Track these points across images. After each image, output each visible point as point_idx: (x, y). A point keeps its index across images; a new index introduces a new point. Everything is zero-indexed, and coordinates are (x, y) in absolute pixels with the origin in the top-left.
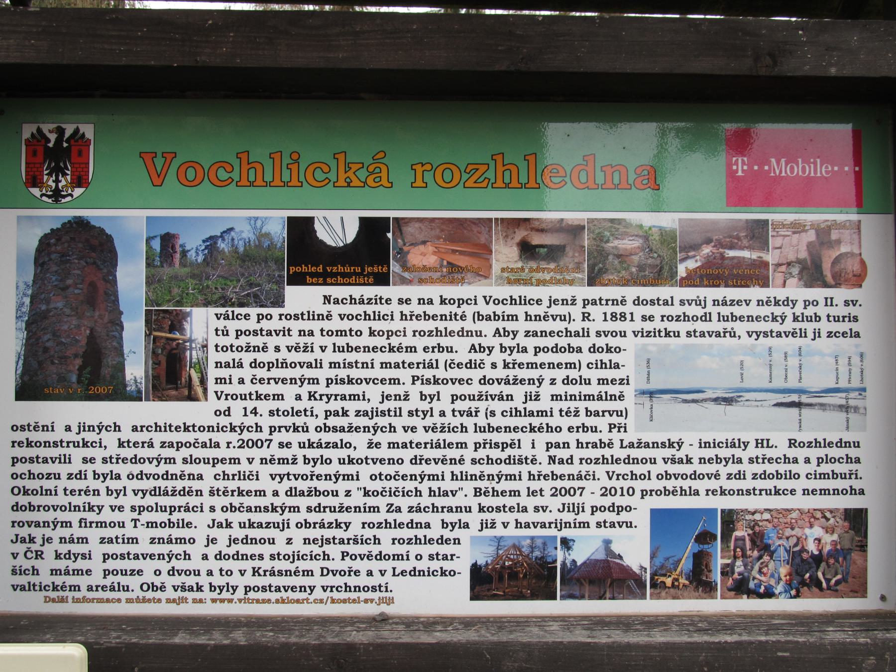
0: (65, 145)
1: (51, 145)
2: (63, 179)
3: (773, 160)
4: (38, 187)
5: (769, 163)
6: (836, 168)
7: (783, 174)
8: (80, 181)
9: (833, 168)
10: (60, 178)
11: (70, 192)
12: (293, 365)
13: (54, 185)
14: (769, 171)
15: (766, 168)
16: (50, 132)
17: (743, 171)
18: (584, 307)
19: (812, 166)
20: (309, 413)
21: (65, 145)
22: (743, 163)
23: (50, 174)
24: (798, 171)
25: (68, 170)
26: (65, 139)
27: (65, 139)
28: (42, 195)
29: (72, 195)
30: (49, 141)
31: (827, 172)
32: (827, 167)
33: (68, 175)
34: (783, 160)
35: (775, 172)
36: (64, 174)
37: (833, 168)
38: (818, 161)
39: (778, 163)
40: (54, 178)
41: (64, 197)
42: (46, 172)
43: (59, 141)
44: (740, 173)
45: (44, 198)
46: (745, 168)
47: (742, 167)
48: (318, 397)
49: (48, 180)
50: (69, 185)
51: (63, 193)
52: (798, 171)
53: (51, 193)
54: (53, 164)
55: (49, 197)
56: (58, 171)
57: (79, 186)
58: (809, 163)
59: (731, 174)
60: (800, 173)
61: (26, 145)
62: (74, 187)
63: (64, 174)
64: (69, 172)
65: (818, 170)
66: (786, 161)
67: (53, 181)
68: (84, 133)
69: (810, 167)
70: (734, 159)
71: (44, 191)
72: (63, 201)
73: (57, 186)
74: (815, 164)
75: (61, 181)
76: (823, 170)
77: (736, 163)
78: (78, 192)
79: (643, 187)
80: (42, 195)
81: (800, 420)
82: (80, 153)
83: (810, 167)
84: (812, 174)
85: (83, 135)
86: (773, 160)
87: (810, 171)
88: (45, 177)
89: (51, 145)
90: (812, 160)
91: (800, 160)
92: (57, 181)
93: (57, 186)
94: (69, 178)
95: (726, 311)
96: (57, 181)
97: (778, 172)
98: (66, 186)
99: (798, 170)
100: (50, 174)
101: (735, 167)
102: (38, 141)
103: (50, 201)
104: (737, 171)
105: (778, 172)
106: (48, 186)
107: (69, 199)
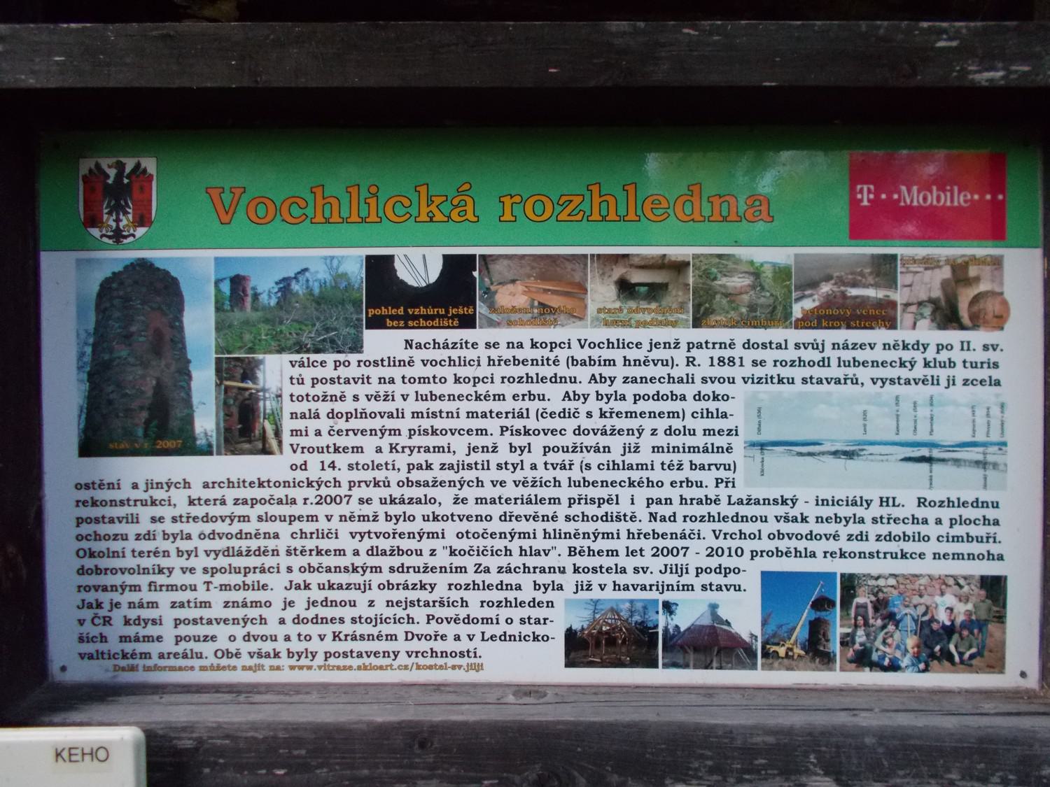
0: (126, 181)
1: (110, 181)
3: (904, 188)
5: (899, 193)
7: (915, 203)
8: (143, 219)
9: (972, 197)
10: (121, 217)
11: (132, 231)
13: (114, 225)
14: (899, 200)
15: (896, 196)
17: (869, 200)
18: (689, 351)
19: (948, 194)
20: (390, 467)
21: (126, 181)
22: (869, 191)
23: (110, 213)
24: (918, 197)
26: (125, 174)
28: (102, 236)
29: (133, 236)
30: (108, 177)
31: (965, 201)
32: (965, 196)
33: (129, 213)
34: (915, 189)
35: (905, 202)
36: (126, 213)
37: (972, 197)
38: (956, 189)
39: (909, 191)
40: (114, 217)
41: (126, 237)
42: (105, 211)
43: (120, 175)
45: (105, 240)
46: (872, 196)
48: (343, 638)
49: (108, 219)
50: (131, 224)
51: (124, 233)
52: (946, 200)
54: (113, 203)
55: (109, 237)
56: (118, 209)
57: (142, 225)
58: (944, 191)
59: (854, 203)
60: (935, 203)
62: (136, 227)
63: (126, 213)
64: (130, 211)
69: (946, 196)
70: (859, 187)
71: (104, 232)
72: (125, 241)
73: (118, 226)
74: (952, 192)
75: (121, 221)
76: (962, 199)
77: (861, 191)
78: (141, 231)
80: (102, 236)
83: (946, 196)
84: (948, 204)
85: (145, 170)
86: (904, 188)
87: (945, 200)
88: (105, 217)
89: (110, 181)
90: (948, 188)
91: (934, 188)
93: (118, 226)
94: (130, 217)
96: (118, 221)
98: (127, 225)
99: (932, 199)
100: (110, 213)
101: (859, 196)
103: (110, 242)
104: (861, 200)
105: (908, 201)
107: (131, 239)
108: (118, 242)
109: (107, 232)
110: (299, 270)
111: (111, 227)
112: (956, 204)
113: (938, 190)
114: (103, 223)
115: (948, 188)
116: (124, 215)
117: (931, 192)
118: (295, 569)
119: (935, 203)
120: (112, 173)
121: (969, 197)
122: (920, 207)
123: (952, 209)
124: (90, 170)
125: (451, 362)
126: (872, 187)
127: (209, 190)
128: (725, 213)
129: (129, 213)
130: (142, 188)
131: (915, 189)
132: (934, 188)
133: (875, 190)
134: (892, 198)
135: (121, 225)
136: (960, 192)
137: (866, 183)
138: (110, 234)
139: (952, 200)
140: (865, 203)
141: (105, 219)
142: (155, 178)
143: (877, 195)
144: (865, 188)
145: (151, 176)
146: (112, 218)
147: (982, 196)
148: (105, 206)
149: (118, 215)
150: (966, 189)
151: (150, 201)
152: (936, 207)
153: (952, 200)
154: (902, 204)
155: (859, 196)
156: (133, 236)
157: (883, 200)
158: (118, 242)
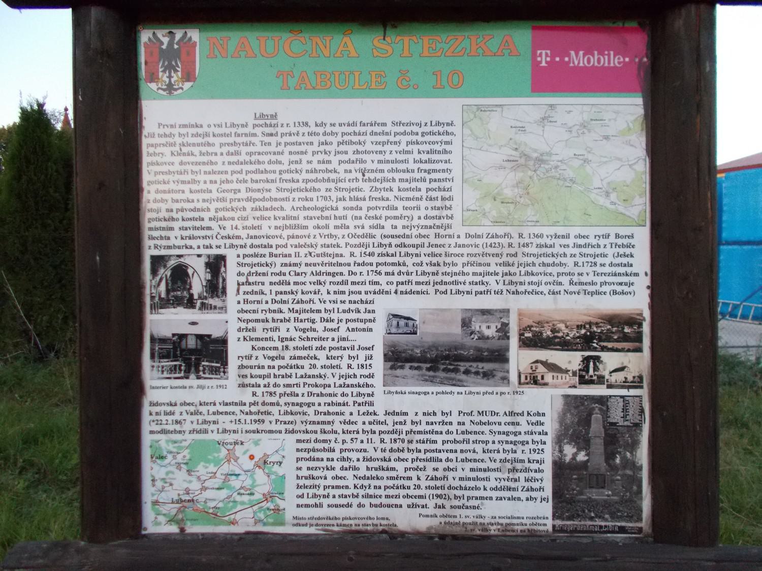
0: (176, 47)
1: (164, 47)
2: (175, 75)
3: (573, 53)
4: (155, 82)
5: (569, 56)
6: (627, 59)
7: (581, 64)
8: (189, 76)
9: (624, 59)
10: (173, 74)
11: (180, 85)
12: (468, 246)
13: (167, 80)
14: (569, 62)
15: (567, 59)
16: (163, 36)
17: (546, 62)
19: (606, 57)
21: (176, 47)
22: (547, 55)
23: (164, 71)
24: (594, 62)
25: (179, 67)
26: (175, 42)
27: (175, 42)
28: (158, 89)
29: (182, 89)
30: (162, 43)
31: (619, 63)
32: (619, 59)
33: (178, 71)
34: (581, 53)
35: (573, 63)
36: (176, 71)
37: (624, 59)
38: (612, 53)
39: (577, 54)
40: (167, 74)
41: (176, 90)
42: (161, 70)
43: (171, 44)
44: (544, 64)
45: (161, 92)
46: (548, 59)
47: (546, 59)
49: (162, 76)
50: (180, 80)
51: (175, 87)
52: (594, 62)
53: (165, 87)
54: (166, 63)
55: (164, 90)
56: (170, 68)
57: (188, 80)
58: (603, 55)
59: (535, 64)
60: (596, 64)
61: (145, 47)
62: (183, 82)
63: (176, 71)
64: (179, 69)
65: (613, 60)
66: (583, 54)
67: (167, 77)
68: (191, 37)
69: (604, 59)
70: (539, 52)
71: (160, 86)
72: (175, 93)
73: (170, 81)
74: (609, 55)
75: (173, 77)
76: (616, 61)
77: (541, 55)
78: (188, 85)
79: (326, 73)
80: (158, 89)
81: (186, 388)
82: (188, 54)
83: (604, 59)
84: (606, 65)
85: (190, 38)
86: (573, 53)
87: (604, 61)
88: (161, 74)
89: (164, 47)
90: (606, 52)
91: (596, 53)
92: (170, 77)
93: (170, 81)
94: (179, 74)
95: (258, 214)
96: (170, 77)
97: (576, 63)
98: (177, 81)
99: (594, 61)
100: (164, 71)
101: (539, 59)
102: (154, 43)
103: (164, 93)
104: (541, 62)
105: (576, 63)
106: (163, 81)
107: (180, 91)
108: (170, 93)
109: (162, 86)
110: (187, 123)
111: (165, 82)
112: (612, 65)
113: (598, 54)
114: (159, 79)
115: (606, 52)
116: (174, 73)
117: (593, 56)
118: (367, 423)
119: (596, 64)
120: (165, 40)
121: (622, 60)
122: (585, 67)
123: (609, 68)
124: (150, 39)
125: (440, 190)
126: (549, 52)
127: (254, 56)
128: (352, 77)
129: (178, 71)
130: (188, 54)
131: (581, 53)
132: (596, 53)
133: (551, 54)
134: (555, 59)
135: (173, 80)
136: (615, 56)
137: (544, 49)
138: (164, 87)
139: (609, 62)
140: (544, 64)
141: (160, 77)
142: (198, 44)
143: (553, 57)
144: (544, 52)
145: (195, 43)
146: (165, 75)
147: (562, 60)
148: (160, 66)
149: (170, 73)
150: (618, 54)
151: (194, 62)
152: (596, 67)
153: (609, 62)
154: (571, 65)
155: (539, 59)
156: (182, 89)
157: (557, 62)
158: (170, 93)
